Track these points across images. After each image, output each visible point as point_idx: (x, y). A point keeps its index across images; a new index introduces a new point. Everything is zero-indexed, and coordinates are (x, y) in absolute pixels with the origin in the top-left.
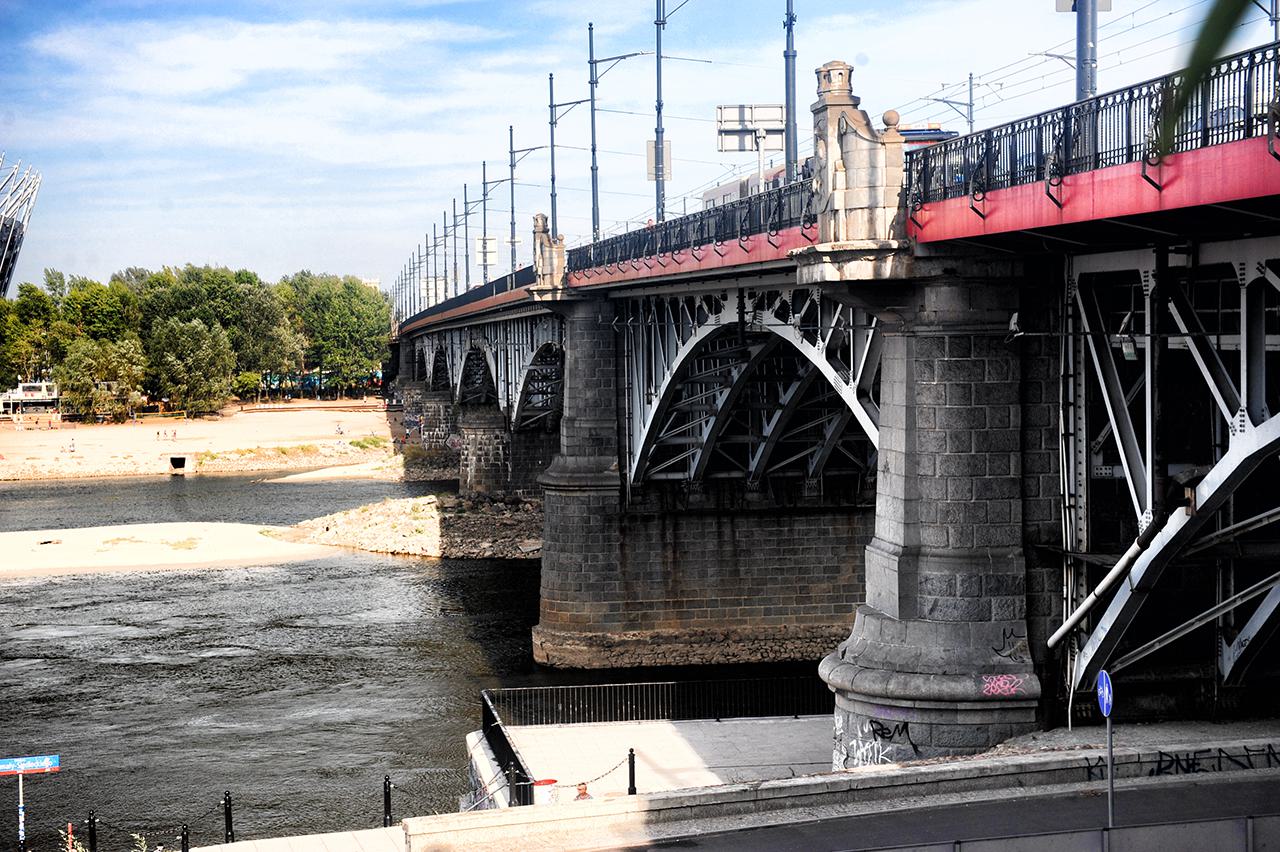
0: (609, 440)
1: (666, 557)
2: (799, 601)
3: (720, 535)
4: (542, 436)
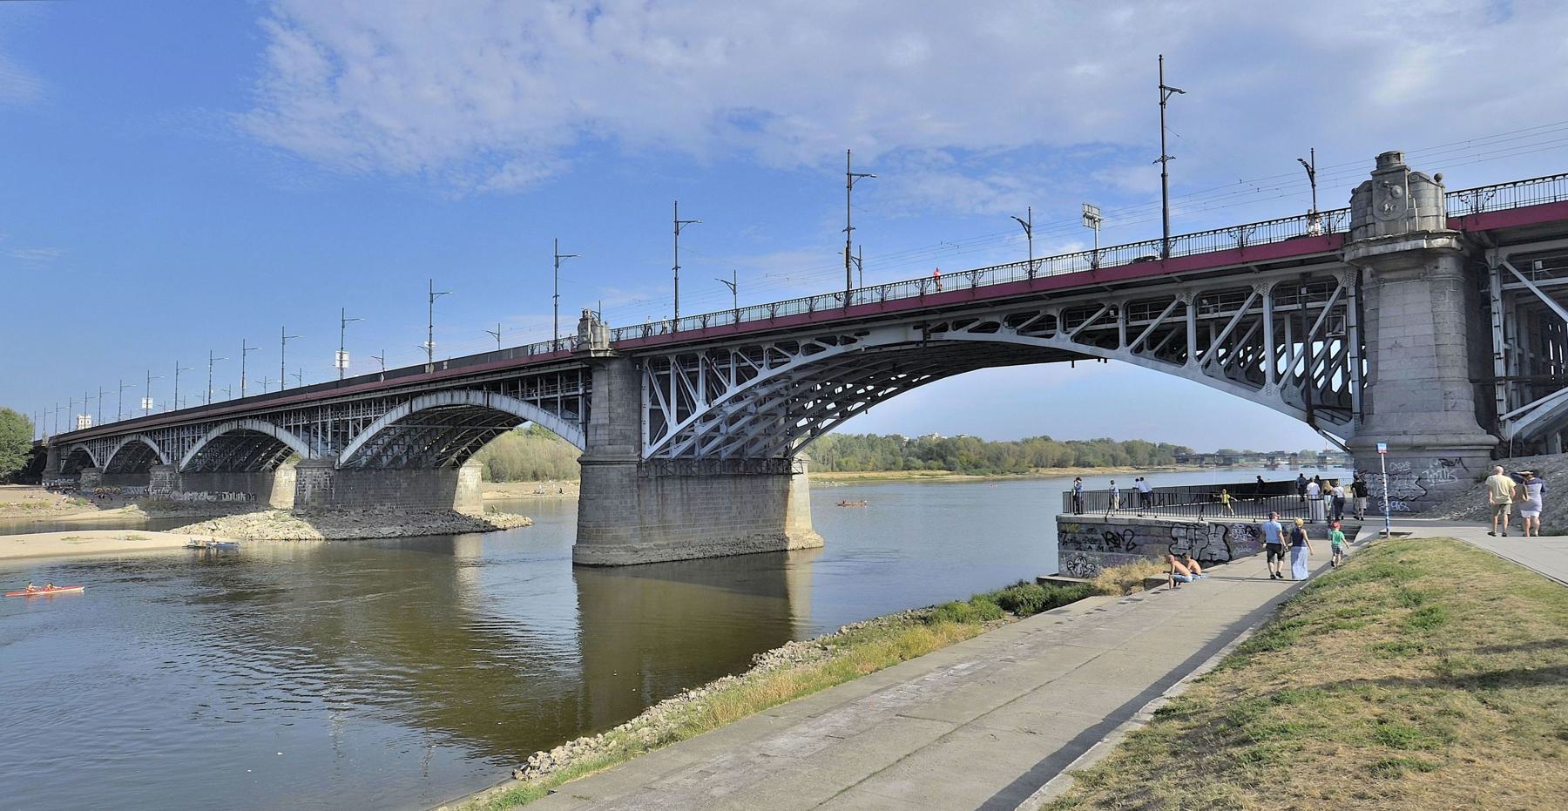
2: (715, 524)
3: (682, 489)
4: (353, 473)
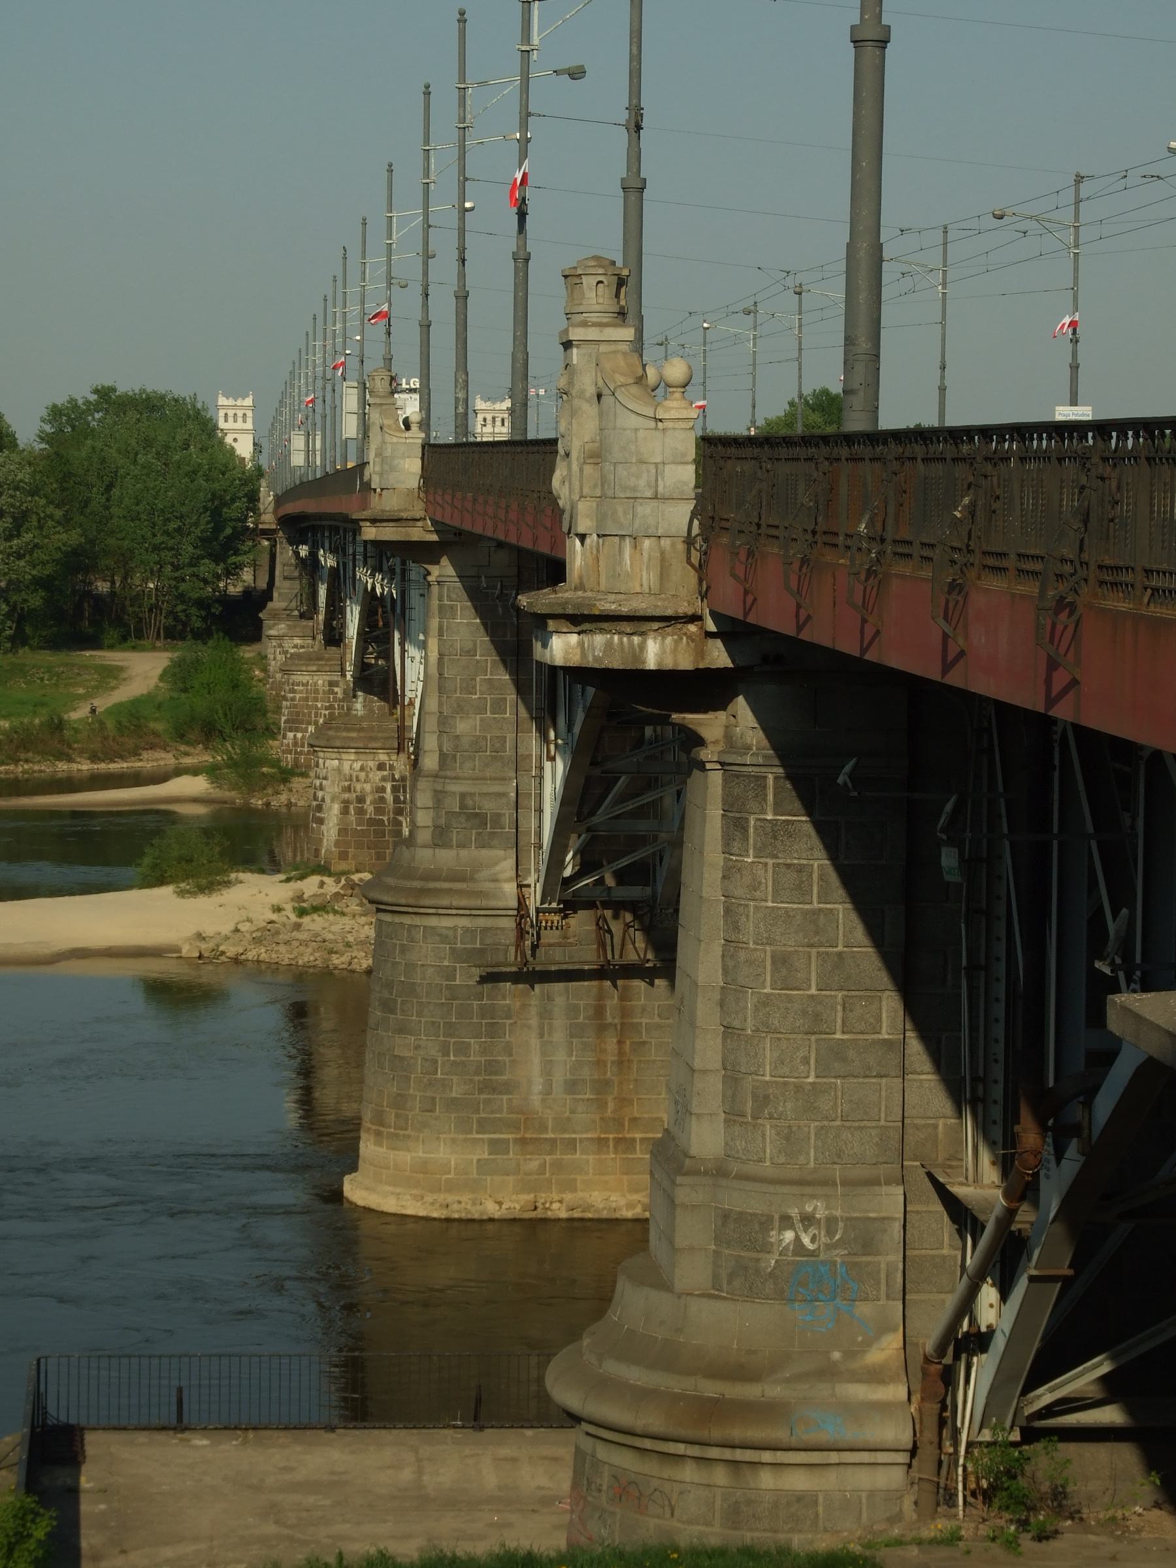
0: (497, 818)
1: (603, 1051)
